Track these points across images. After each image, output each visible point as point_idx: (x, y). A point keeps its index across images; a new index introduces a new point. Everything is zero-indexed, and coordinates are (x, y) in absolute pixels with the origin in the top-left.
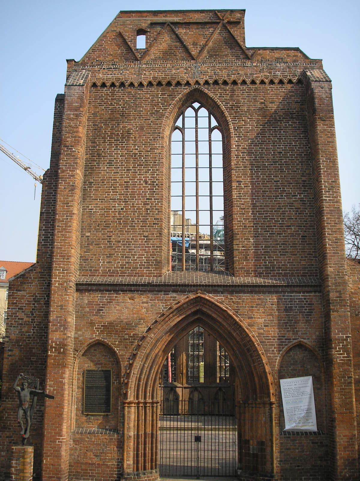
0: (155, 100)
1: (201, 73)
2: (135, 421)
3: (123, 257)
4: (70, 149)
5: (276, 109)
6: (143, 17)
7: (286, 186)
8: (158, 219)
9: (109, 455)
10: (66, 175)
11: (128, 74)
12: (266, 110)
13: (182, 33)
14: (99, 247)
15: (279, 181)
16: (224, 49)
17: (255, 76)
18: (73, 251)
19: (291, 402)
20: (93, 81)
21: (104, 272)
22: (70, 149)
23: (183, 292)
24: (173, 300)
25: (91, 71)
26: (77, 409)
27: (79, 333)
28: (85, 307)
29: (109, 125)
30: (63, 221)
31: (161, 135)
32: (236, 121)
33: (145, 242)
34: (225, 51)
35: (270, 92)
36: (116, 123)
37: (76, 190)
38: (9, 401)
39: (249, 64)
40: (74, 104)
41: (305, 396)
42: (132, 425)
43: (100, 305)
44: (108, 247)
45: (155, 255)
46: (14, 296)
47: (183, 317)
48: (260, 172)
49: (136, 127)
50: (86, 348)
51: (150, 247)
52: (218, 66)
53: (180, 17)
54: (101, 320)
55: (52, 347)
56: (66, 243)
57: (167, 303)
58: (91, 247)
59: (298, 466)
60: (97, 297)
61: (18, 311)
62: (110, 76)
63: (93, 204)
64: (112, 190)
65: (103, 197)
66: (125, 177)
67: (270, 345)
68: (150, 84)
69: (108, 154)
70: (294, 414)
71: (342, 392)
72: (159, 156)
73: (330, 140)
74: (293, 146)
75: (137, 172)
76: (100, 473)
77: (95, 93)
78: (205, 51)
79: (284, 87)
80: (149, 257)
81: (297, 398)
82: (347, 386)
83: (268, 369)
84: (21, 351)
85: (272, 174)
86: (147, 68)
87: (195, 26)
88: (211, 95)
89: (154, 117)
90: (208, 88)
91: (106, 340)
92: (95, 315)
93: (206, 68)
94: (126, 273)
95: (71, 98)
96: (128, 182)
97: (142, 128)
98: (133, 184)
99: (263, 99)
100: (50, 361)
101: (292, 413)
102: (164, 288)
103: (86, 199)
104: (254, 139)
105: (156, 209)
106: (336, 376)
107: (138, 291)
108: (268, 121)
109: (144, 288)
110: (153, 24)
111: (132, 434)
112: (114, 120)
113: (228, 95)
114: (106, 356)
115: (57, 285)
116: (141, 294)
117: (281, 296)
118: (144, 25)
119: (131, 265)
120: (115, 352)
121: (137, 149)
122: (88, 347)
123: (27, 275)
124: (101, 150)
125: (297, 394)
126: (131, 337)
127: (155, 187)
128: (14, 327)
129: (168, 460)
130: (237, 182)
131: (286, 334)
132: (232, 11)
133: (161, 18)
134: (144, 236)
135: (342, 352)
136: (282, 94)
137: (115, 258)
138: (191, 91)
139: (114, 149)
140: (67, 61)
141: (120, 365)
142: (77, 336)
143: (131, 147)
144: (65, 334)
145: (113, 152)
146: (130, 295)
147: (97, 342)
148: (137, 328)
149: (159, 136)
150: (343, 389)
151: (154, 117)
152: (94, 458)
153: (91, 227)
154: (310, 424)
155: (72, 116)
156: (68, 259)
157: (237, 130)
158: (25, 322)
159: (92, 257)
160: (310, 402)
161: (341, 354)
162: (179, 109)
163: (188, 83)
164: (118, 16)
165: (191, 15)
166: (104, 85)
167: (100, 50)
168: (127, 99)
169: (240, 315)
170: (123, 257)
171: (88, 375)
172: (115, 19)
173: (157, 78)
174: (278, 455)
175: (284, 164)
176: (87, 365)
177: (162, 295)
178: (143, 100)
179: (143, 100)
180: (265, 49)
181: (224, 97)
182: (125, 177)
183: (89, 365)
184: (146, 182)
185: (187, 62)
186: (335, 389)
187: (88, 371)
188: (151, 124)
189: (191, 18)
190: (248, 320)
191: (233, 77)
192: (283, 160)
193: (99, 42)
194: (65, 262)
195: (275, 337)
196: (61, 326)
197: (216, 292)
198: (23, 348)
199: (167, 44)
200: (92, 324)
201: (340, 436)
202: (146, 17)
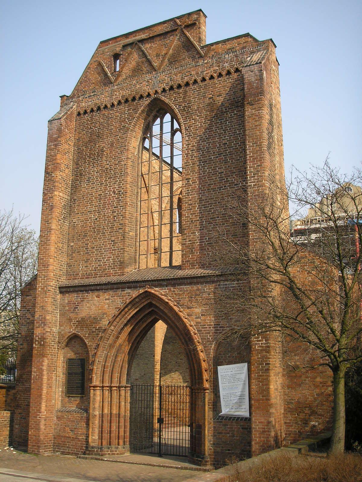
0: (123, 117)
1: (160, 82)
2: (100, 402)
3: (96, 261)
4: (51, 175)
5: (223, 101)
6: (118, 42)
7: (229, 176)
8: (122, 224)
9: (80, 430)
10: (47, 198)
11: (103, 98)
12: (214, 104)
13: (147, 48)
14: (79, 254)
15: (223, 172)
16: (182, 53)
17: (205, 73)
18: (51, 260)
19: (227, 388)
20: (78, 111)
21: (83, 275)
22: (51, 175)
23: (136, 287)
24: (128, 296)
25: (76, 102)
26: (62, 392)
27: (62, 328)
28: (66, 306)
29: (88, 147)
30: (45, 236)
31: (126, 148)
32: (187, 121)
33: (113, 246)
34: (183, 55)
35: (218, 86)
36: (94, 144)
37: (54, 209)
38: (21, 385)
39: (201, 62)
40: (54, 136)
41: (239, 383)
42: (97, 405)
43: (76, 303)
44: (86, 253)
45: (119, 256)
46: (24, 300)
47: (138, 309)
48: (206, 166)
49: (108, 144)
50: (67, 340)
51: (116, 250)
52: (174, 72)
53: (146, 33)
54: (77, 316)
55: (36, 341)
56: (46, 254)
57: (123, 298)
58: (74, 255)
59: (229, 450)
60: (73, 297)
61: (26, 313)
62: (90, 103)
63: (76, 218)
64: (90, 203)
65: (83, 211)
66: (99, 191)
67: (206, 333)
68: (119, 103)
69: (88, 172)
70: (230, 400)
71: (260, 379)
72: (125, 167)
73: (257, 123)
74: (237, 134)
75: (107, 185)
76: (74, 446)
77: (79, 120)
78: (166, 60)
79: (231, 78)
80: (115, 259)
81: (232, 384)
82: (265, 373)
83: (202, 355)
84: (28, 344)
85: (217, 167)
86: (118, 88)
87: (158, 38)
88: (167, 101)
89: (121, 133)
90: (164, 95)
91: (79, 333)
92: (71, 313)
93: (164, 76)
94: (98, 275)
95: (53, 131)
96: (101, 195)
97: (112, 145)
98: (105, 196)
99: (211, 94)
100: (35, 352)
101: (228, 399)
102: (120, 286)
103: (71, 214)
104: (202, 135)
105: (121, 215)
106: (254, 362)
107: (102, 289)
108: (215, 115)
109: (106, 287)
110: (125, 47)
111: (97, 413)
112: (93, 142)
113: (181, 97)
114: (82, 347)
115: (40, 290)
116: (105, 292)
117: (216, 285)
118: (118, 49)
119: (101, 267)
120: (85, 343)
121: (108, 164)
122: (68, 339)
123: (32, 283)
124: (83, 170)
125: (233, 381)
126: (97, 329)
127: (121, 195)
128: (24, 325)
129: (178, 441)
130: (186, 179)
131: (220, 322)
132: (189, 14)
133: (131, 39)
134: (112, 241)
135: (260, 339)
136: (230, 85)
137: (90, 262)
138: (151, 101)
139: (92, 168)
140: (60, 97)
141: (89, 354)
142: (60, 330)
143: (104, 163)
144: (44, 330)
145: (91, 170)
146: (96, 293)
147: (74, 335)
148: (101, 322)
149: (125, 148)
150: (261, 376)
151: (121, 133)
152: (70, 433)
153: (74, 237)
154: (243, 410)
155: (52, 147)
156: (47, 267)
157: (188, 129)
158: (31, 321)
159: (75, 263)
160: (244, 388)
161: (260, 341)
162: (145, 119)
163: (149, 95)
164: (99, 47)
165: (155, 29)
166: (85, 112)
167: (86, 81)
168: (102, 121)
169: (181, 306)
170: (96, 261)
171: (70, 362)
172: (97, 50)
173: (125, 96)
174: (211, 438)
175: (228, 155)
176: (69, 355)
177: (119, 292)
178: (114, 119)
179: (114, 119)
180: (217, 43)
181: (177, 100)
182: (99, 191)
183: (71, 355)
184: (114, 192)
185: (149, 75)
186: (253, 376)
187: (70, 359)
188: (119, 139)
189: (156, 31)
190: (187, 310)
191: (186, 79)
192: (228, 150)
193: (85, 74)
194: (45, 270)
195: (210, 325)
196: (42, 323)
197: (161, 286)
198: (29, 342)
199: (135, 62)
200: (70, 320)
201: (256, 422)
202: (120, 41)
